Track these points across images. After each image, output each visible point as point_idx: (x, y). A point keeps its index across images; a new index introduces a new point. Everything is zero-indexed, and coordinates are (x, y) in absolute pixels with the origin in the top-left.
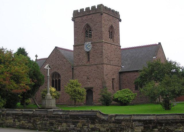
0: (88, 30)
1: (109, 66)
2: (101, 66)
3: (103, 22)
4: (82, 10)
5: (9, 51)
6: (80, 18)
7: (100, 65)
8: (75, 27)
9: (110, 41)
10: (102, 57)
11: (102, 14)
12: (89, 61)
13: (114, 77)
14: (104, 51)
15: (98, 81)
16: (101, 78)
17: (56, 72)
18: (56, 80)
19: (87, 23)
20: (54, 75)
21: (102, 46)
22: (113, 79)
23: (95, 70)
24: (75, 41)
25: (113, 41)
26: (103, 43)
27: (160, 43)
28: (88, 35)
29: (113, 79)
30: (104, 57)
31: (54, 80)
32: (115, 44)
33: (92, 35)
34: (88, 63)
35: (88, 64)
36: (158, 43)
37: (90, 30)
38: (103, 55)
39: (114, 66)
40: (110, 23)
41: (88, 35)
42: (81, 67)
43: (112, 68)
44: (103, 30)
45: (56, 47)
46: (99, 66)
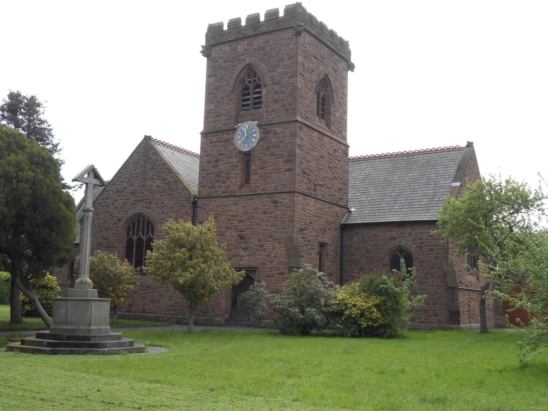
0: (251, 86)
1: (312, 202)
2: (285, 199)
3: (300, 59)
4: (235, 23)
5: (16, 93)
6: (226, 48)
7: (284, 196)
8: (209, 76)
9: (319, 124)
10: (290, 170)
11: (298, 34)
12: (247, 180)
13: (326, 239)
14: (298, 151)
15: (274, 248)
16: (285, 240)
17: (140, 215)
18: (140, 240)
19: (247, 61)
20: (134, 224)
21: (293, 135)
22: (322, 245)
23: (264, 213)
24: (206, 117)
25: (328, 126)
26: (298, 124)
27: (470, 145)
28: (248, 100)
29: (322, 245)
30: (298, 170)
31: (135, 238)
32: (334, 137)
33: (264, 99)
34: (243, 190)
35: (246, 190)
36: (463, 144)
37: (259, 86)
38: (295, 165)
39: (327, 205)
40: (321, 68)
41: (248, 100)
42: (219, 200)
43: (321, 209)
44: (299, 85)
45: (147, 139)
46: (278, 198)
